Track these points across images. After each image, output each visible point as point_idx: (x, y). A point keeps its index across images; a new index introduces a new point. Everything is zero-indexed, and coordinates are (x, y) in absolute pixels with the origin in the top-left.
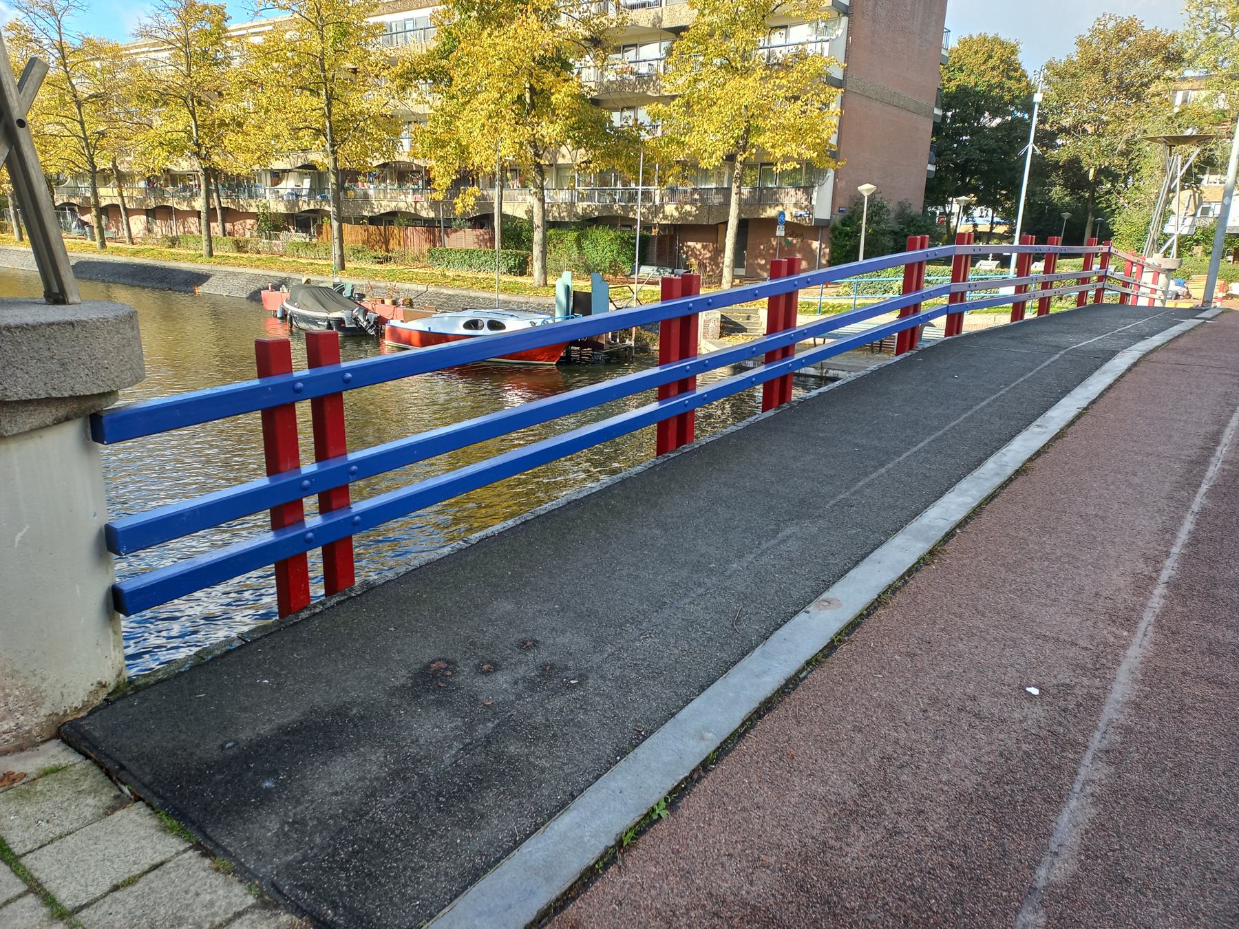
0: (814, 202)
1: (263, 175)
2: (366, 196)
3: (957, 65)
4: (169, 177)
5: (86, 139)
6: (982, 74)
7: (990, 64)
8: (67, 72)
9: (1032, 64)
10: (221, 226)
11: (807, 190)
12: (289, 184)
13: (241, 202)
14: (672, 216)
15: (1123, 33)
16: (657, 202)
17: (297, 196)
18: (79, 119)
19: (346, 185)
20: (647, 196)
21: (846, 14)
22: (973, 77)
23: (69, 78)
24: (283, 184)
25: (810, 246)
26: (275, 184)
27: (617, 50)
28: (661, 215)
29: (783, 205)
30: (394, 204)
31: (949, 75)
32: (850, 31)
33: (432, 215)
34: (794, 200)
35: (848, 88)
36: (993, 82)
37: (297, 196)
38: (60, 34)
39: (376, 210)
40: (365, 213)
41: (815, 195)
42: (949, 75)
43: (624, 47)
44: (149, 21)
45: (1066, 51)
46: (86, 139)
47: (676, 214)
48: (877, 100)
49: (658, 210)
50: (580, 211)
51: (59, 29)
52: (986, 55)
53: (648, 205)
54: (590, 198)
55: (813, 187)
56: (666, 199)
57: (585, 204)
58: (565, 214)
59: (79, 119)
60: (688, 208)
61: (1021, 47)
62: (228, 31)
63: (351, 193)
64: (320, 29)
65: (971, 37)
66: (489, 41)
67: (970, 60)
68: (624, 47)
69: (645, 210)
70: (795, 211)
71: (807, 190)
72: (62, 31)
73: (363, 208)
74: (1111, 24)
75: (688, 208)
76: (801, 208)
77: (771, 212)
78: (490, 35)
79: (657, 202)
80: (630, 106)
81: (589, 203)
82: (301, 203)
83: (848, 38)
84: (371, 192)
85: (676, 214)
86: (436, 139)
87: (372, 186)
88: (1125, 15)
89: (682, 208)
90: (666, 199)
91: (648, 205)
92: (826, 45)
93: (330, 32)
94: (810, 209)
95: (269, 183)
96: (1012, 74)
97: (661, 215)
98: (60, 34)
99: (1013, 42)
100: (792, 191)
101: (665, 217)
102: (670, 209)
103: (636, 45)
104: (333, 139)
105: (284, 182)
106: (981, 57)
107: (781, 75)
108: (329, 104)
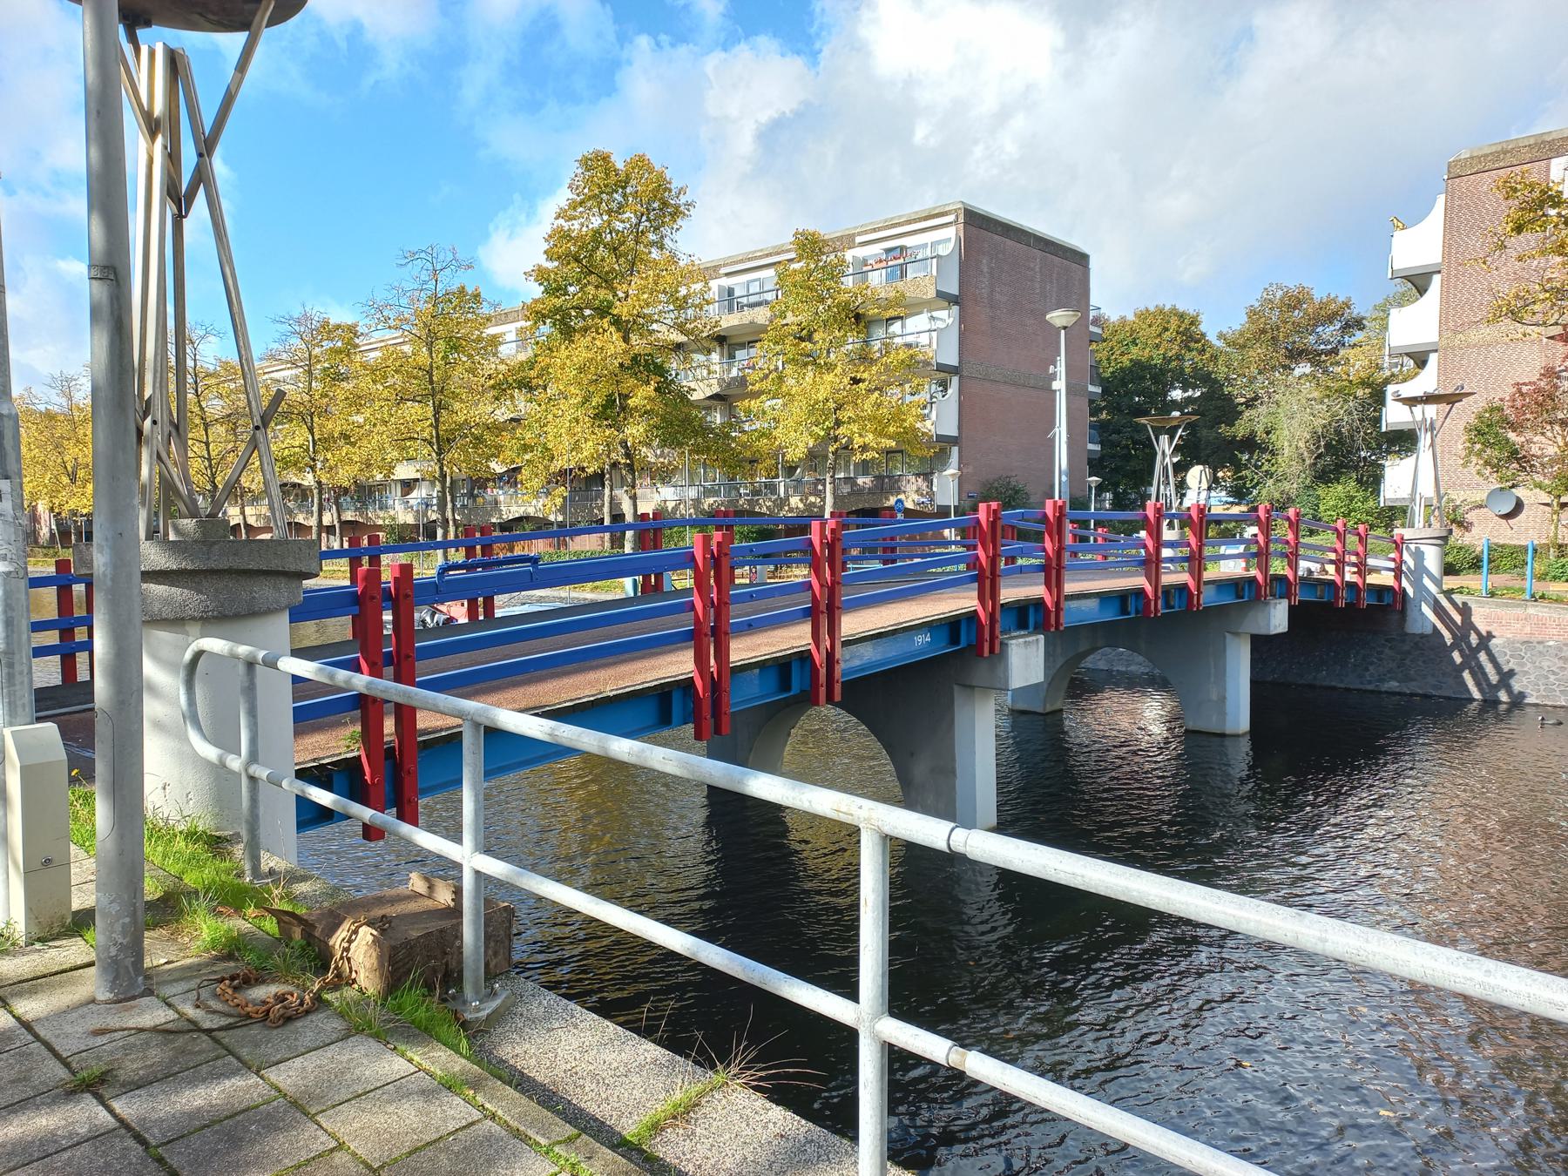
0: (935, 489)
1: (393, 485)
2: (496, 502)
3: (1130, 339)
4: (300, 492)
5: (209, 460)
6: (1157, 346)
7: (1166, 336)
8: (198, 396)
9: (1212, 329)
10: (338, 540)
11: (927, 476)
12: (417, 495)
13: (370, 515)
14: (797, 508)
15: (1294, 301)
16: (782, 495)
17: (427, 506)
18: (205, 440)
19: (476, 492)
20: (772, 488)
21: (956, 303)
22: (1148, 350)
23: (199, 401)
24: (415, 494)
25: (942, 535)
26: (406, 493)
27: (742, 346)
28: (787, 508)
29: (904, 492)
30: (523, 509)
31: (1122, 349)
32: (962, 319)
33: (560, 518)
34: (915, 488)
35: (965, 373)
36: (1170, 354)
37: (427, 506)
38: (195, 360)
39: (504, 517)
40: (494, 520)
41: (935, 481)
42: (1122, 349)
43: (749, 343)
44: (275, 346)
45: (1236, 322)
46: (209, 460)
47: (801, 506)
48: (1005, 382)
49: (783, 502)
50: (706, 507)
51: (195, 355)
52: (1160, 329)
53: (774, 498)
54: (716, 493)
55: (932, 473)
56: (791, 492)
57: (711, 500)
58: (692, 511)
59: (205, 440)
60: (812, 499)
61: (1202, 318)
62: (359, 347)
63: (480, 500)
64: (430, 346)
65: (1147, 310)
66: (567, 353)
67: (1145, 333)
68: (749, 343)
69: (770, 503)
70: (916, 497)
71: (927, 476)
72: (197, 357)
73: (491, 516)
74: (1279, 294)
75: (812, 499)
76: (922, 495)
77: (892, 501)
78: (567, 348)
79: (782, 495)
80: (34, 518)
81: (715, 499)
82: (430, 512)
83: (960, 325)
84: (502, 498)
85: (801, 506)
86: (525, 445)
87: (501, 492)
88: (1292, 283)
89: (807, 499)
90: (791, 492)
91: (774, 498)
92: (934, 334)
93: (441, 345)
94: (931, 495)
95: (399, 494)
96: (1192, 345)
97: (787, 508)
98: (195, 360)
99: (1192, 312)
100: (913, 479)
101: (791, 510)
102: (795, 501)
103: (902, 318)
104: (439, 449)
105: (415, 491)
106: (1155, 330)
107: (862, 368)
108: (437, 413)
